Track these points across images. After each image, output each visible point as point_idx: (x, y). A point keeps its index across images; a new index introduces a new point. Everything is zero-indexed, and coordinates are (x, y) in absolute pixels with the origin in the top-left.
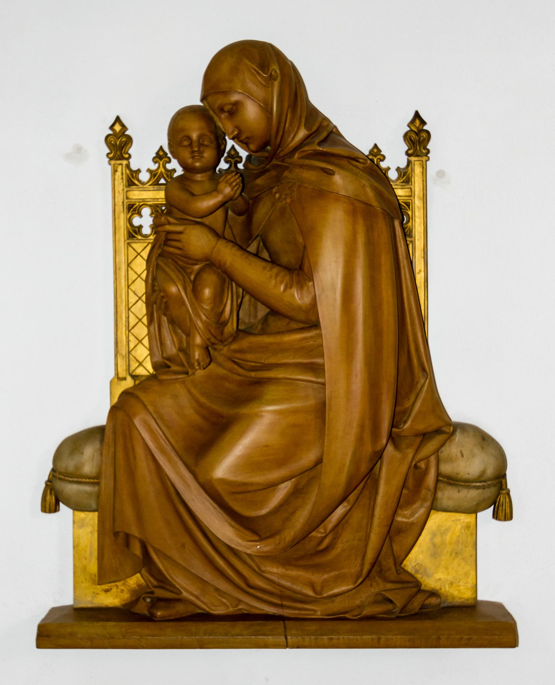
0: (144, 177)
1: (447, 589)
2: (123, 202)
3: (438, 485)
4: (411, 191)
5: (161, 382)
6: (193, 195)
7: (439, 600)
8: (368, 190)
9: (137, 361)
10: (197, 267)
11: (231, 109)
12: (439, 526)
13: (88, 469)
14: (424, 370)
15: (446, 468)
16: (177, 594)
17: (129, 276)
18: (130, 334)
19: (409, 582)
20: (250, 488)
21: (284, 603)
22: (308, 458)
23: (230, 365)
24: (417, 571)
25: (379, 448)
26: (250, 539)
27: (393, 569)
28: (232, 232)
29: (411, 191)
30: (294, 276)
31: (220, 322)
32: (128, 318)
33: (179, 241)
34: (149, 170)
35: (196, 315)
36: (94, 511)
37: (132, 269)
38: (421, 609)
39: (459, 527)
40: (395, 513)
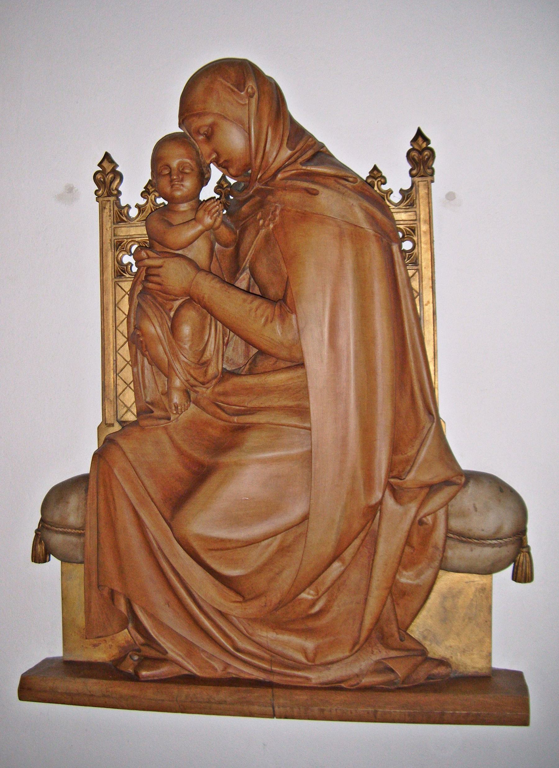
0: (134, 212)
1: (459, 657)
2: (111, 240)
3: (447, 543)
4: (416, 215)
5: (143, 428)
6: (171, 225)
7: (449, 670)
8: (357, 210)
9: (126, 406)
10: (177, 304)
11: (207, 131)
12: (450, 588)
13: (73, 519)
14: (430, 413)
15: (456, 524)
16: (163, 654)
17: (117, 316)
18: (118, 378)
19: (414, 650)
20: (228, 545)
21: (274, 669)
22: (296, 511)
23: (213, 408)
24: (425, 638)
25: (373, 501)
26: (234, 599)
27: (396, 635)
28: (220, 267)
29: (416, 215)
30: (276, 308)
31: (201, 362)
32: (116, 361)
33: (158, 275)
34: (137, 206)
35: (173, 354)
36: (81, 563)
37: (120, 309)
38: (428, 678)
39: (473, 589)
40: (396, 571)
